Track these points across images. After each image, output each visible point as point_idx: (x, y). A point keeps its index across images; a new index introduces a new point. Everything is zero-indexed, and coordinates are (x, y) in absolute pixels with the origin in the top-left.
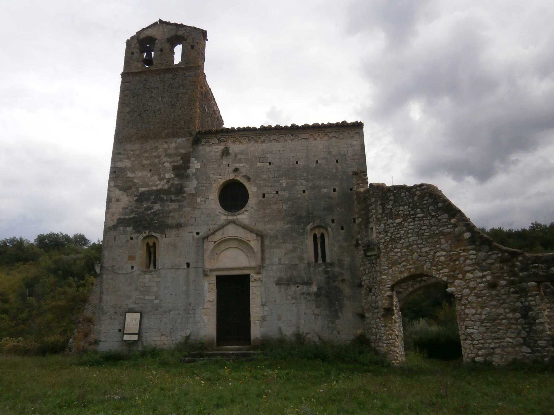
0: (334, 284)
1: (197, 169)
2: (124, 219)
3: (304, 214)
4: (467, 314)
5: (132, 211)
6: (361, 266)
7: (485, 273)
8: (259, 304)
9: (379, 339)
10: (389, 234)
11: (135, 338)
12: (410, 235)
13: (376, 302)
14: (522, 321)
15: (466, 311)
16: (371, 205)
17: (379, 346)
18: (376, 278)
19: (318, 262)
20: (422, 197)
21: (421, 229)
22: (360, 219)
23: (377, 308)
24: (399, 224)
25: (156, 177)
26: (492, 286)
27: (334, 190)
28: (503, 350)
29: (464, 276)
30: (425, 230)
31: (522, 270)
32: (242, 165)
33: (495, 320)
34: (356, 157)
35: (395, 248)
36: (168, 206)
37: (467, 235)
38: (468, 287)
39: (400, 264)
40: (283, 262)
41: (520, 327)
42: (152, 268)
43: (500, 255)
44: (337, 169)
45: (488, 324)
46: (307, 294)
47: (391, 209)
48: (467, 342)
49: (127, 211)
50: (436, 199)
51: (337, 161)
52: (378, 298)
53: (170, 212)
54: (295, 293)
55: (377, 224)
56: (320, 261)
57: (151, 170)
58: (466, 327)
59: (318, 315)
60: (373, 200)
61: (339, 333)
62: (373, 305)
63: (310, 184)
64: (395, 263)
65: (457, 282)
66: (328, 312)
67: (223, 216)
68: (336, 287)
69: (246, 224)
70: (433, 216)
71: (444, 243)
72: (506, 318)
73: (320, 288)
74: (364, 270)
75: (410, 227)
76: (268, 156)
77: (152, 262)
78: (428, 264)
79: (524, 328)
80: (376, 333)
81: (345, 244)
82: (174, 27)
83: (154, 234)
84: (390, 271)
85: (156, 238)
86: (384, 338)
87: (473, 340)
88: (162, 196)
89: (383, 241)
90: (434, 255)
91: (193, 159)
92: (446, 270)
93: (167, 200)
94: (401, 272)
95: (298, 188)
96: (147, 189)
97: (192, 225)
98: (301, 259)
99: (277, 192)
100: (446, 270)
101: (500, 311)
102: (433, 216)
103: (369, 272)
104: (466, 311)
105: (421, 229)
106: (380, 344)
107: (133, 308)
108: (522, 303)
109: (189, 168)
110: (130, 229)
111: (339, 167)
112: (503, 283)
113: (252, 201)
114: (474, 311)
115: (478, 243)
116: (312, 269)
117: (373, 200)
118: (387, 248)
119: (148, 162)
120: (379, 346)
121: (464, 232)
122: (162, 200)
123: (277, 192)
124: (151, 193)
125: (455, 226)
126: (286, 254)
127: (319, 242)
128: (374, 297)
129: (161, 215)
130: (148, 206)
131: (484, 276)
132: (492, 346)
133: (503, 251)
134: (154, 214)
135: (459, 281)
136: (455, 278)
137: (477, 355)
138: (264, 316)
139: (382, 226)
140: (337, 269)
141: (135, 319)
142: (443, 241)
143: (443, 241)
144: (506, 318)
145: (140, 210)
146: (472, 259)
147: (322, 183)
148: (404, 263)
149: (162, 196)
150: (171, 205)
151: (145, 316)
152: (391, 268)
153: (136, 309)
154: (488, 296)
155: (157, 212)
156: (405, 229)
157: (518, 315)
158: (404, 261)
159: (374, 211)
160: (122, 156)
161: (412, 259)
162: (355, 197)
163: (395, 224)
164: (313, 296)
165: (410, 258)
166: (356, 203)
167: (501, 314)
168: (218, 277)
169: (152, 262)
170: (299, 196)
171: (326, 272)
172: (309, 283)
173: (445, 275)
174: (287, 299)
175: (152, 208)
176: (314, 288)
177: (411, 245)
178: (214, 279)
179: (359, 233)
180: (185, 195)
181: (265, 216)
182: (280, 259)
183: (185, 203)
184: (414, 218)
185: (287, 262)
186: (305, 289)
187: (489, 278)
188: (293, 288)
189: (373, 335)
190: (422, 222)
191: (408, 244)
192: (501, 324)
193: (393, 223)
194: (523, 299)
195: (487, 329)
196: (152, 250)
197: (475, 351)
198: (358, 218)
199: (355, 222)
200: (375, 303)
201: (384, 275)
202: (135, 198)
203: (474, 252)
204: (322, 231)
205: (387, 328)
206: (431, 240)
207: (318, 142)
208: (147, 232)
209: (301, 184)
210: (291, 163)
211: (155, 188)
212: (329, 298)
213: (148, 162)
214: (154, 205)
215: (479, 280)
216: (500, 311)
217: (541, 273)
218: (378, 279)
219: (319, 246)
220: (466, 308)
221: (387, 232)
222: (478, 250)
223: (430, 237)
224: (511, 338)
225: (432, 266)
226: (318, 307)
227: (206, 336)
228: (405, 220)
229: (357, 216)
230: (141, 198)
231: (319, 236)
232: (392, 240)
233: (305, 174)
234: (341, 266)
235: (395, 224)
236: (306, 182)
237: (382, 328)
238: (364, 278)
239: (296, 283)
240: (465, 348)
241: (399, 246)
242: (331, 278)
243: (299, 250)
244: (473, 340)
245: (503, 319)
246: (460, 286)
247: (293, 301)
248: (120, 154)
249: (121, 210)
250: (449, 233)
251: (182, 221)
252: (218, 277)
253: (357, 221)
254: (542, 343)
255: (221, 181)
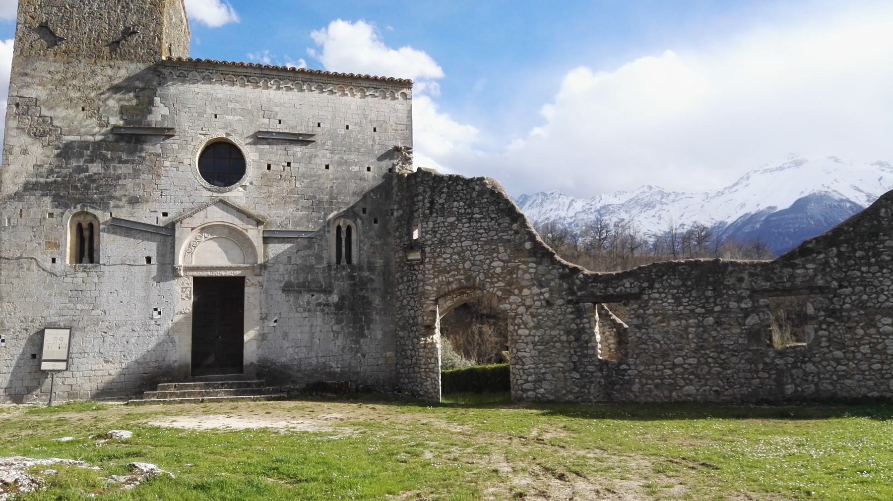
0: (361, 294)
1: (164, 116)
2: (37, 183)
3: (326, 198)
4: (521, 336)
5: (51, 172)
6: (398, 272)
7: (543, 290)
8: (257, 317)
9: (416, 363)
10: (438, 235)
11: (62, 366)
12: (463, 239)
13: (415, 317)
14: (575, 344)
15: (520, 332)
16: (417, 195)
17: (414, 372)
18: (417, 288)
19: (342, 264)
20: (481, 194)
21: (477, 233)
22: (401, 212)
23: (416, 324)
24: (452, 224)
25: (94, 120)
26: (549, 304)
27: (369, 169)
28: (553, 376)
29: (521, 291)
30: (481, 234)
31: (580, 289)
32: (237, 118)
33: (547, 343)
34: (399, 127)
35: (445, 253)
36: (115, 169)
37: (528, 245)
38: (524, 305)
39: (448, 272)
40: (293, 261)
41: (572, 351)
42: (86, 258)
43: (561, 271)
44: (374, 140)
45: (540, 347)
46: (325, 305)
47: (443, 205)
48: (517, 366)
49: (43, 170)
50: (498, 198)
51: (375, 130)
52: (419, 312)
53: (119, 178)
54: (308, 303)
55: (423, 221)
56: (344, 262)
57: (83, 109)
58: (518, 350)
59: (338, 333)
60: (421, 189)
61: (364, 356)
62: (411, 321)
63: (336, 157)
64: (445, 271)
65: (512, 298)
66: (351, 330)
67: (204, 192)
68: (363, 297)
69: (242, 205)
70: (492, 219)
71: (503, 252)
72: (560, 341)
73: (342, 298)
74: (402, 277)
75: (465, 229)
76: (276, 109)
77: (86, 253)
78: (482, 276)
79: (576, 352)
80: (412, 356)
81: (378, 243)
82: (423, 401)
83: (91, 211)
84: (436, 281)
85: (95, 216)
86: (422, 362)
87: (524, 364)
88: (104, 152)
89: (429, 242)
90: (489, 265)
91: (157, 99)
92: (502, 284)
93: (112, 159)
94: (449, 283)
95: (318, 161)
96: (77, 138)
97: (155, 201)
98: (319, 258)
99: (289, 164)
100: (502, 284)
101: (554, 333)
102: (492, 219)
103: (408, 281)
104: (520, 332)
105: (477, 233)
106: (417, 369)
107: (55, 323)
108: (577, 324)
109: (150, 112)
110: (48, 200)
111: (377, 138)
112: (560, 302)
113: (251, 173)
114: (527, 332)
115: (539, 255)
116: (333, 273)
117: (421, 189)
118: (435, 252)
119: (78, 94)
120: (414, 372)
121: (525, 241)
122: (105, 160)
123: (289, 164)
124: (84, 145)
125: (516, 232)
126: (298, 251)
127: (344, 236)
128: (412, 311)
129: (103, 182)
130: (79, 166)
131: (541, 293)
132: (543, 371)
133: (565, 267)
134: (91, 179)
135: (515, 297)
136: (511, 293)
137: (527, 381)
138: (264, 334)
139: (431, 224)
140: (366, 274)
141: (61, 339)
142: (501, 249)
143: (501, 249)
144: (560, 341)
145: (65, 171)
146: (531, 273)
147: (352, 157)
148: (453, 272)
149: (104, 152)
150: (120, 168)
151: (73, 332)
152: (435, 277)
153: (62, 324)
154: (544, 317)
155: (96, 177)
156: (458, 231)
157: (572, 338)
158: (454, 270)
159: (421, 204)
160: (28, 79)
161: (464, 268)
162: (395, 181)
163: (446, 224)
164: (333, 308)
165: (461, 266)
166: (396, 189)
167: (555, 336)
168: (196, 279)
169: (86, 253)
170: (320, 172)
171: (351, 277)
172: (328, 291)
173: (500, 289)
174: (297, 311)
175: (87, 170)
176: (335, 298)
177: (463, 251)
178: (191, 281)
179: (397, 229)
180: (143, 154)
181: (270, 197)
182: (289, 258)
183: (143, 167)
184: (470, 219)
185: (299, 262)
186: (322, 298)
187: (547, 295)
188: (306, 297)
189: (407, 358)
190: (479, 224)
191: (460, 249)
192: (554, 347)
193: (444, 222)
194: (578, 321)
195: (539, 352)
196: (86, 234)
197: (525, 377)
198: (397, 210)
199: (392, 214)
200: (413, 319)
201: (428, 285)
202: (56, 152)
203: (534, 265)
204: (349, 222)
205: (427, 350)
206: (486, 247)
207: (349, 98)
208: (79, 206)
209: (324, 156)
210: (311, 124)
211: (90, 138)
212: (353, 311)
213: (78, 94)
214: (90, 165)
215: (536, 298)
216: (554, 333)
217: (598, 294)
218: (420, 289)
219: (343, 242)
220: (519, 328)
221: (435, 232)
222: (538, 263)
223: (486, 243)
224: (562, 362)
225: (486, 278)
226: (339, 322)
227: (175, 361)
228: (458, 220)
229: (396, 207)
230: (66, 152)
231: (344, 229)
232: (441, 242)
233: (329, 143)
234: (371, 268)
235: (446, 224)
236: (331, 153)
237: (421, 350)
238: (401, 287)
239: (310, 291)
240: (514, 374)
241: (449, 250)
242: (358, 285)
243: (316, 246)
244: (524, 364)
245: (556, 342)
246: (516, 303)
247: (306, 314)
248: (26, 74)
249: (31, 168)
250: (509, 241)
251: (139, 193)
252: (196, 279)
253: (395, 214)
254: (591, 368)
255: (246, 180)
